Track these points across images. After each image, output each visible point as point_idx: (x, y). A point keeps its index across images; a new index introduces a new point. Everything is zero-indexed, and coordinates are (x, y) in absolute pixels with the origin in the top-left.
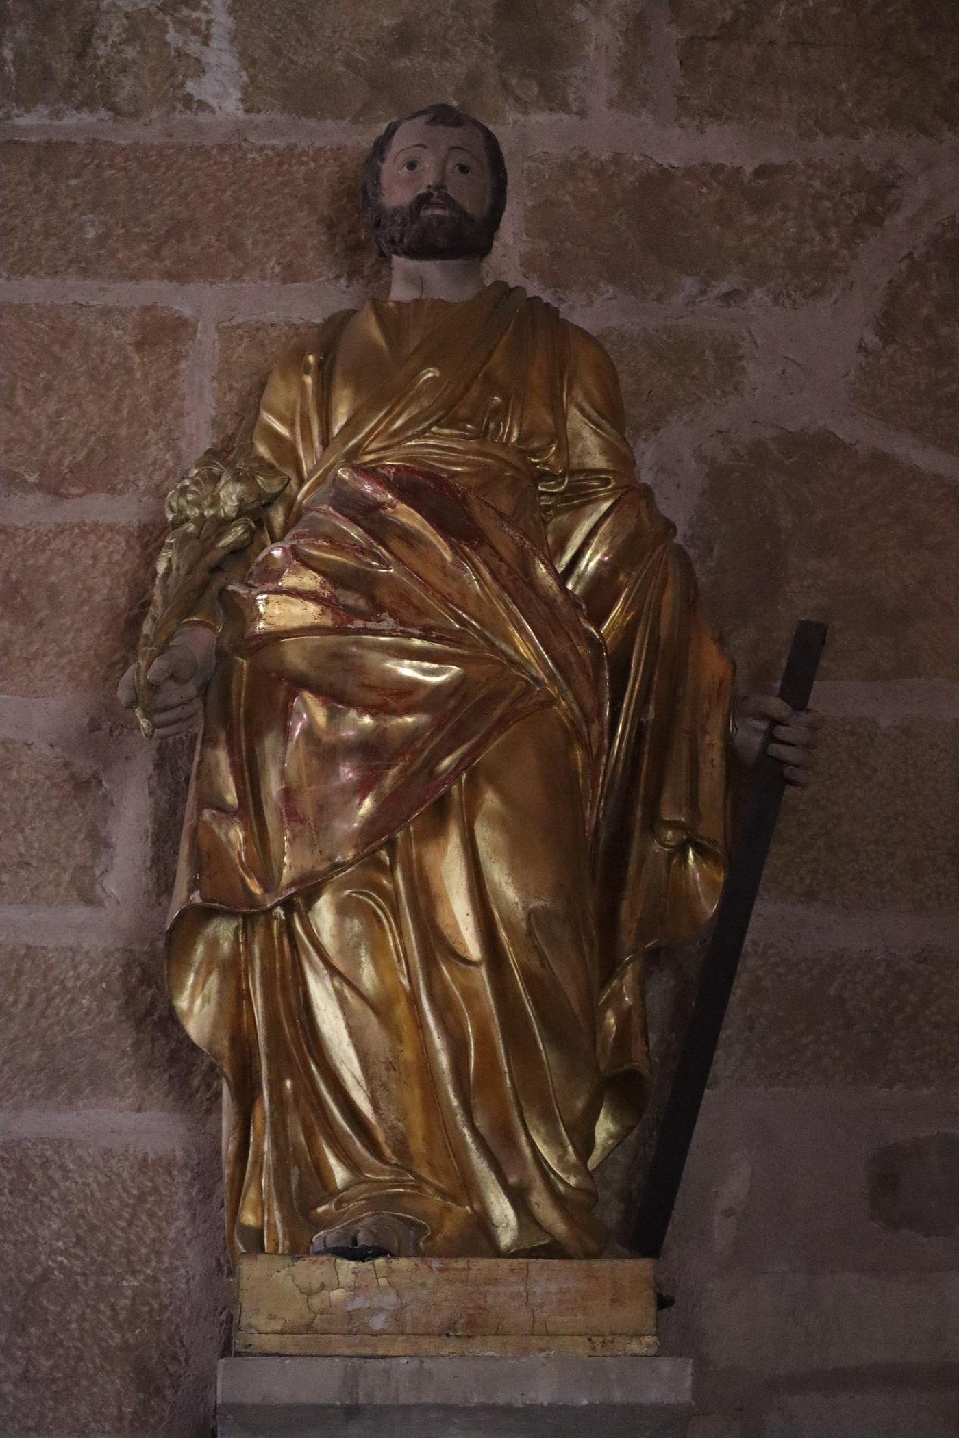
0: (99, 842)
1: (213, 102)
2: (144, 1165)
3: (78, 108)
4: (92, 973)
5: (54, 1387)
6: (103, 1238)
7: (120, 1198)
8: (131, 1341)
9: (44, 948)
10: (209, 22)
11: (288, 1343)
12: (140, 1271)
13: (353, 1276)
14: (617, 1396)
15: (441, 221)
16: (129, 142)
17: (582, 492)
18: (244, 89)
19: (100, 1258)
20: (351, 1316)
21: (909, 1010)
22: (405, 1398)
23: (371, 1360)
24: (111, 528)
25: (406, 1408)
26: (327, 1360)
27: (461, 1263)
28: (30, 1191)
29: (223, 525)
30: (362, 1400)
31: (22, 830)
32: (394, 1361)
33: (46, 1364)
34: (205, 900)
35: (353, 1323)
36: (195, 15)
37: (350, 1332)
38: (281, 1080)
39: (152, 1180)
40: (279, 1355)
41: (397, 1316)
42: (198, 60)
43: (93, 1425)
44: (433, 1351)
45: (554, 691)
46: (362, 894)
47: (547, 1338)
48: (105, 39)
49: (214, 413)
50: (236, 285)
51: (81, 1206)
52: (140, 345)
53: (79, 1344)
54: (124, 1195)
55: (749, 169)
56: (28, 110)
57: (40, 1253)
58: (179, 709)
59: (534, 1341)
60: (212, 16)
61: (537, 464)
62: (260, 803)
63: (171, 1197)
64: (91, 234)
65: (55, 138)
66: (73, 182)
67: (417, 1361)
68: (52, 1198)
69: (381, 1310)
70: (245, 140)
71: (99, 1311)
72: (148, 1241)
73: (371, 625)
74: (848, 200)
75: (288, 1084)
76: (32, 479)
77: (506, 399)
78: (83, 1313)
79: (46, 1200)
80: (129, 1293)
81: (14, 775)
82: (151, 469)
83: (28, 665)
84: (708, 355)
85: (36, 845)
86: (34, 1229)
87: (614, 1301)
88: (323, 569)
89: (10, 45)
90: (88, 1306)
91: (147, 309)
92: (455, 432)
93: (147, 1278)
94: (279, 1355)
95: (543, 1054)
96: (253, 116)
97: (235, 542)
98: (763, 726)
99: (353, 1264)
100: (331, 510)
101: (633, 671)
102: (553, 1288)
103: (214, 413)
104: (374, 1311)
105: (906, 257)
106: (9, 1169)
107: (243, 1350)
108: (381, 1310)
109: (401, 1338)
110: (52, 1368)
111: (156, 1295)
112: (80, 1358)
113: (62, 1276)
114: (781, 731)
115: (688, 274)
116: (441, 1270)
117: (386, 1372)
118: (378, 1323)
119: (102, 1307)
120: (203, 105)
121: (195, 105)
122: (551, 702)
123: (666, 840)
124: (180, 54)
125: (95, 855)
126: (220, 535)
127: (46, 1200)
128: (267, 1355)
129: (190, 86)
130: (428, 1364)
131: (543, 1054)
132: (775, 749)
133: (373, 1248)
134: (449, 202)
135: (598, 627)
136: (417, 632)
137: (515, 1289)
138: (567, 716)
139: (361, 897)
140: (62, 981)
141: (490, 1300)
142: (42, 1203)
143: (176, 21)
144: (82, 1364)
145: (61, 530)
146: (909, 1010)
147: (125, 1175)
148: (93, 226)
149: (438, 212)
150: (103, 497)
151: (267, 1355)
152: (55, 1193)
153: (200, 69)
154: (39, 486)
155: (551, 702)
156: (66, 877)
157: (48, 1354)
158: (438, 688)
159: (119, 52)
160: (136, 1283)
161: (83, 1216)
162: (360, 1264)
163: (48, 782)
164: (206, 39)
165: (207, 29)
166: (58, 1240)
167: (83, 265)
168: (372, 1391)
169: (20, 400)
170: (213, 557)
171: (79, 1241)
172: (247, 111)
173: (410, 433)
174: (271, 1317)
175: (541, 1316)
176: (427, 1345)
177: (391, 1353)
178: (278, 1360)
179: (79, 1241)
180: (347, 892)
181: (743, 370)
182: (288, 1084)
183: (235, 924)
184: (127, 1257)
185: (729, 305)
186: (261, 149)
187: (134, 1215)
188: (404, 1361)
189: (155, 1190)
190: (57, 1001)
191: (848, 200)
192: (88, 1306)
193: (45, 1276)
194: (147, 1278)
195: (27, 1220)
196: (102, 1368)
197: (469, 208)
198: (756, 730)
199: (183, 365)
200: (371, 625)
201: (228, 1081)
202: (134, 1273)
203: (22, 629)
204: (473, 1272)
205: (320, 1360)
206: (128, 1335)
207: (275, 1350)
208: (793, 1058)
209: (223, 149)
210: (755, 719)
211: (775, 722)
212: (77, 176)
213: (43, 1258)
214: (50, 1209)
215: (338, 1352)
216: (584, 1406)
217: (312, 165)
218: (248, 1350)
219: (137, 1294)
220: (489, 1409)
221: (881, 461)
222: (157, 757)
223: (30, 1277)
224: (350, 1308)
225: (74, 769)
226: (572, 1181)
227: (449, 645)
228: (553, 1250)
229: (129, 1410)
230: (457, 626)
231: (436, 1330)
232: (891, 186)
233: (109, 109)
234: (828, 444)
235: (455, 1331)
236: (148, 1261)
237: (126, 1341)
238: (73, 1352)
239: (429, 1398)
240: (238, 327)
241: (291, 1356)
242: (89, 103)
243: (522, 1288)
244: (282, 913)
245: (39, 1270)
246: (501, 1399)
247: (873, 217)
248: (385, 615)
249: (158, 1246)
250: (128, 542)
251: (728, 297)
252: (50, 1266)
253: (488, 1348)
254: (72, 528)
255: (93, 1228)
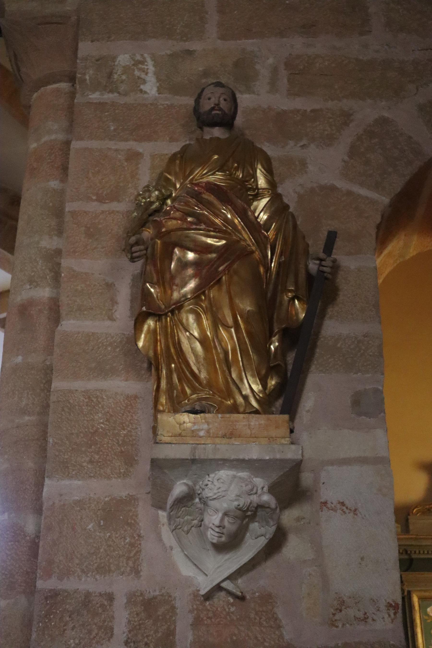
0: (114, 302)
1: (148, 92)
2: (128, 397)
3: (108, 93)
4: (112, 340)
5: (99, 464)
6: (114, 419)
7: (120, 407)
8: (123, 450)
9: (97, 333)
10: (148, 69)
11: (173, 440)
12: (126, 429)
13: (194, 419)
14: (278, 456)
15: (218, 114)
16: (124, 102)
17: (261, 195)
18: (158, 87)
19: (114, 425)
20: (193, 431)
21: (362, 351)
22: (211, 456)
23: (199, 445)
24: (118, 212)
25: (211, 460)
26: (186, 445)
27: (228, 415)
28: (92, 405)
29: (152, 203)
30: (197, 457)
31: (91, 299)
32: (207, 445)
33: (97, 457)
34: (147, 309)
35: (194, 433)
36: (143, 67)
37: (193, 436)
38: (170, 365)
39: (130, 402)
40: (170, 443)
41: (208, 431)
42: (144, 80)
43: (111, 476)
44: (219, 442)
45: (254, 248)
46: (196, 307)
47: (255, 439)
48: (116, 73)
49: (149, 179)
50: (156, 143)
51: (108, 409)
52: (127, 160)
53: (107, 451)
54: (121, 406)
55: (309, 110)
56: (94, 93)
57: (95, 423)
58: (139, 252)
59: (251, 439)
60: (148, 67)
61: (248, 185)
62: (155, 399)
63: (136, 407)
64: (112, 128)
65: (102, 101)
66: (106, 114)
67: (214, 445)
68: (99, 407)
69: (202, 430)
70: (158, 102)
71: (114, 441)
72: (129, 420)
73: (198, 227)
74: (338, 119)
75: (173, 365)
76: (94, 198)
77: (238, 165)
78: (109, 442)
79: (97, 408)
80: (123, 435)
81: (88, 283)
82: (130, 195)
83: (93, 251)
84: (297, 163)
85: (95, 303)
86: (94, 416)
87: (276, 427)
88: (182, 211)
89: (88, 75)
90: (110, 439)
91: (129, 150)
92: (223, 174)
93: (129, 431)
94: (170, 443)
95: (252, 356)
96: (160, 95)
97: (156, 207)
98: (318, 262)
99: (194, 415)
100: (186, 195)
101: (277, 247)
102: (257, 423)
103: (149, 179)
104: (199, 430)
105: (356, 135)
106: (85, 398)
107: (159, 442)
108: (202, 430)
109: (209, 438)
110: (99, 458)
111: (131, 436)
112: (108, 455)
113: (102, 431)
114: (324, 263)
115: (290, 140)
116: (222, 418)
117: (205, 449)
118: (202, 433)
119: (114, 439)
120: (146, 92)
121: (143, 92)
122: (253, 252)
123: (288, 296)
124: (139, 78)
125: (113, 306)
126: (151, 206)
127: (97, 408)
128: (167, 443)
129: (142, 87)
130: (218, 446)
131: (252, 356)
132: (321, 268)
133: (200, 410)
134: (220, 109)
135: (267, 233)
136: (212, 229)
137: (245, 423)
138: (258, 256)
139: (195, 308)
140: (103, 343)
141: (237, 427)
142: (96, 409)
143: (137, 69)
144: (108, 457)
145: (103, 212)
146: (362, 351)
147: (122, 400)
148: (112, 126)
149: (218, 112)
150: (116, 203)
151: (167, 443)
152: (100, 406)
153: (144, 82)
154: (96, 200)
155: (253, 252)
156: (104, 312)
157: (98, 454)
158: (218, 247)
159: (121, 77)
160: (125, 433)
161: (109, 413)
162: (196, 415)
163: (98, 285)
164: (147, 74)
165: (147, 71)
166: (101, 419)
167: (109, 137)
168: (200, 454)
169: (90, 175)
170: (150, 211)
171: (108, 420)
172: (159, 94)
173: (209, 174)
174: (168, 432)
175: (253, 432)
176: (217, 440)
177: (206, 443)
178: (170, 445)
179: (108, 420)
180: (191, 307)
181: (308, 168)
182: (173, 365)
183: (156, 319)
184: (122, 425)
185: (303, 149)
186: (163, 105)
187: (124, 412)
188: (210, 445)
189: (131, 405)
190: (101, 348)
191: (338, 119)
192: (110, 439)
193: (96, 431)
194: (129, 431)
195: (91, 414)
196: (115, 458)
197: (227, 111)
198: (315, 264)
199: (140, 165)
200: (198, 227)
201: (154, 366)
202: (124, 429)
203: (91, 240)
204: (232, 418)
205: (184, 445)
206: (122, 448)
207: (169, 442)
208: (327, 365)
209: (151, 104)
210: (315, 260)
211: (321, 260)
212: (108, 112)
213: (96, 425)
214: (98, 410)
215: (189, 442)
216: (267, 460)
217: (178, 109)
218: (161, 442)
219: (125, 435)
220: (238, 460)
221: (349, 193)
222: (132, 278)
223: (92, 431)
224: (193, 429)
225: (107, 281)
226: (261, 395)
227: (222, 234)
228: (256, 412)
229: (123, 471)
230: (224, 228)
231: (220, 436)
232: (352, 115)
233: (118, 93)
234: (333, 188)
235: (226, 436)
236: (129, 426)
237: (122, 450)
238: (105, 453)
239: (218, 457)
240: (156, 155)
241: (174, 444)
242: (111, 91)
243: (247, 423)
244: (170, 315)
245: (95, 429)
246: (241, 457)
247: (346, 124)
248: (202, 224)
249: (132, 421)
250: (123, 216)
251: (303, 146)
252: (98, 428)
253: (236, 442)
254: (106, 212)
255: (111, 416)
